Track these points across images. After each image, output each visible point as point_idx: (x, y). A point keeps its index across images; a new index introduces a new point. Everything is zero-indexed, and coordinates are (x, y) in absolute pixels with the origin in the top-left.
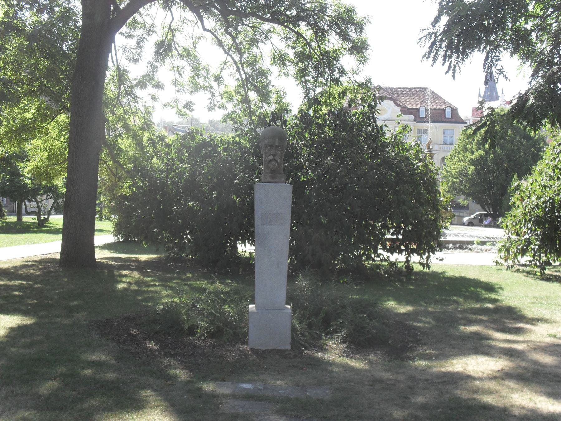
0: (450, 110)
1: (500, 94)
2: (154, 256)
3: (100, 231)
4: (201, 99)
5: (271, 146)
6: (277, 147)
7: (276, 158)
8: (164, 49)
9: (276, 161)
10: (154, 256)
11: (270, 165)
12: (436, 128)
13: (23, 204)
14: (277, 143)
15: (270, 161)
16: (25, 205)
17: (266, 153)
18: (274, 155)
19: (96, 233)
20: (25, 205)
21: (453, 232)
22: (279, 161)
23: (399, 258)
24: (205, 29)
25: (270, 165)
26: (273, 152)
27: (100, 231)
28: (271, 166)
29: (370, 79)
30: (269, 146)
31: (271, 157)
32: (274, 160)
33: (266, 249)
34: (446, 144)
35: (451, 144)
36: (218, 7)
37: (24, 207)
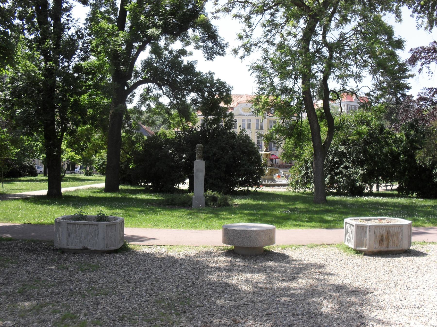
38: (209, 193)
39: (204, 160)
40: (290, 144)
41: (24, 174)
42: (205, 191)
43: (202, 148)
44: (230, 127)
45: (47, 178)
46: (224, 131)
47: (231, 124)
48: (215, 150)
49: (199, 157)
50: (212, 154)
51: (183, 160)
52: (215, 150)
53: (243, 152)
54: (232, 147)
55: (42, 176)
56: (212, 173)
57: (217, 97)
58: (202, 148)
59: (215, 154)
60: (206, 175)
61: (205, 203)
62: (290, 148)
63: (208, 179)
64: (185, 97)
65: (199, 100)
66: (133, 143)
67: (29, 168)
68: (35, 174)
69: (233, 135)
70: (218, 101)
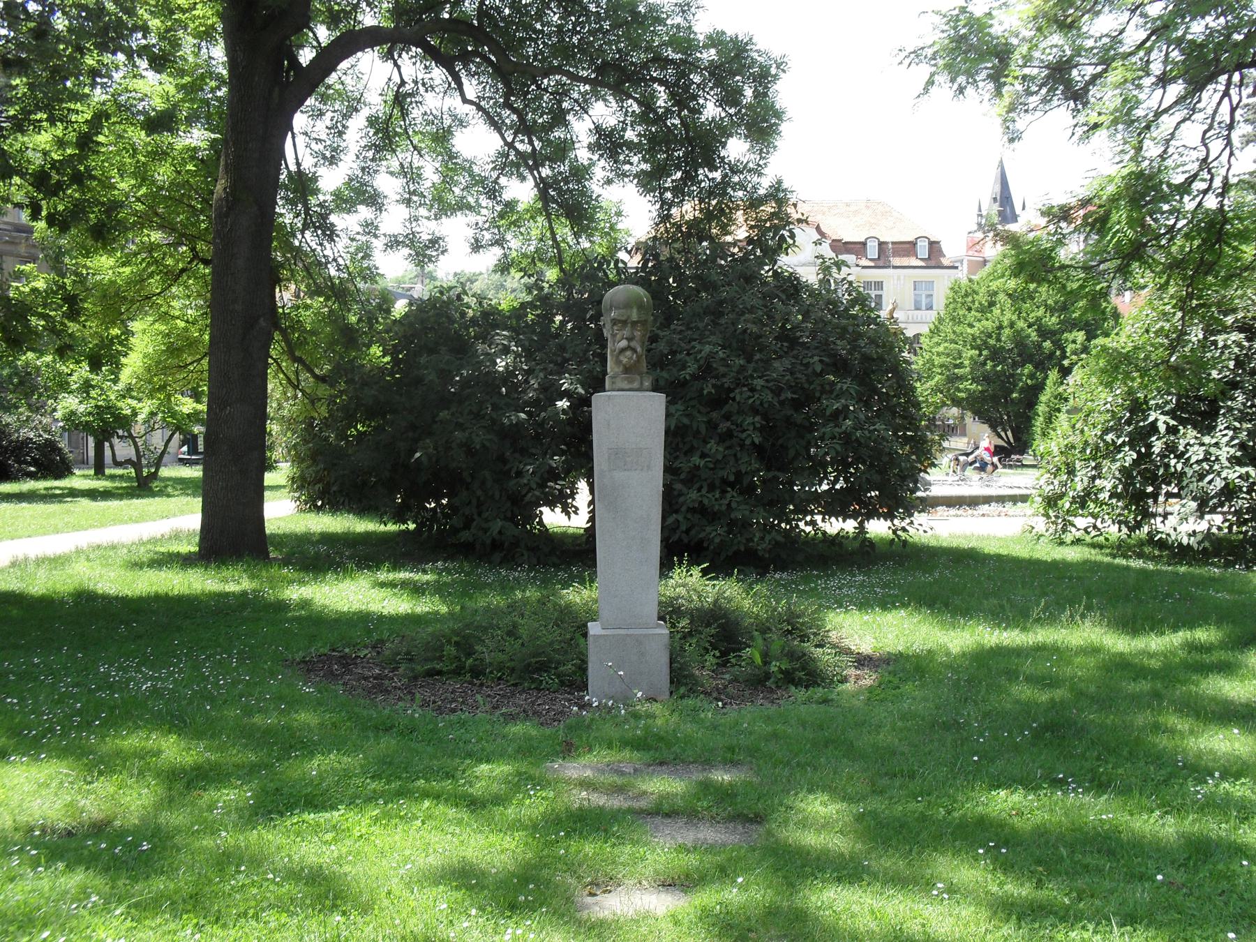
0: (927, 244)
1: (1018, 209)
2: (392, 527)
3: (272, 488)
4: (456, 230)
5: (624, 323)
6: (634, 324)
7: (633, 344)
8: (385, 135)
9: (634, 350)
10: (392, 527)
11: (622, 358)
12: (899, 279)
13: (107, 444)
14: (635, 317)
15: (623, 350)
16: (112, 447)
17: (614, 336)
18: (629, 340)
19: (267, 494)
20: (112, 447)
21: (940, 479)
22: (639, 349)
23: (834, 526)
24: (465, 101)
25: (622, 358)
26: (626, 332)
27: (272, 488)
28: (625, 360)
29: (779, 182)
30: (620, 321)
31: (624, 343)
32: (629, 348)
33: (615, 497)
34: (917, 309)
35: (930, 308)
36: (493, 58)
37: (108, 452)
38: (691, 584)
39: (656, 388)
40: (939, 354)
41: (19, 471)
42: (666, 566)
43: (641, 306)
44: (771, 254)
45: (196, 472)
46: (745, 272)
47: (775, 230)
48: (707, 348)
49: (627, 370)
50: (692, 368)
51: (563, 404)
52: (707, 348)
53: (840, 366)
54: (789, 338)
55: (85, 477)
56: (696, 460)
57: (711, 110)
58: (641, 306)
59: (707, 369)
60: (670, 470)
61: (666, 670)
62: (941, 366)
63: (678, 486)
64: (566, 124)
65: (630, 135)
66: (349, 338)
67: (39, 447)
68: (61, 469)
69: (791, 286)
70: (719, 133)
